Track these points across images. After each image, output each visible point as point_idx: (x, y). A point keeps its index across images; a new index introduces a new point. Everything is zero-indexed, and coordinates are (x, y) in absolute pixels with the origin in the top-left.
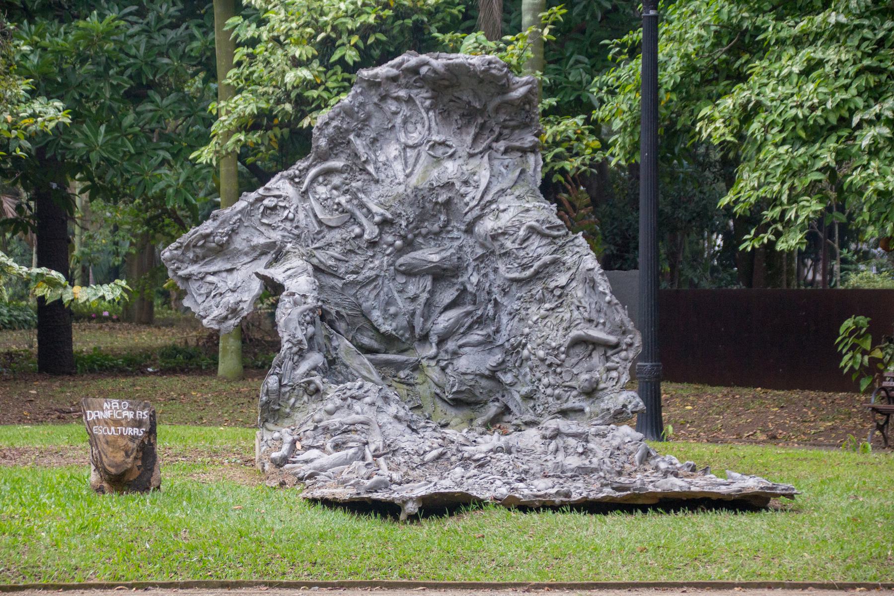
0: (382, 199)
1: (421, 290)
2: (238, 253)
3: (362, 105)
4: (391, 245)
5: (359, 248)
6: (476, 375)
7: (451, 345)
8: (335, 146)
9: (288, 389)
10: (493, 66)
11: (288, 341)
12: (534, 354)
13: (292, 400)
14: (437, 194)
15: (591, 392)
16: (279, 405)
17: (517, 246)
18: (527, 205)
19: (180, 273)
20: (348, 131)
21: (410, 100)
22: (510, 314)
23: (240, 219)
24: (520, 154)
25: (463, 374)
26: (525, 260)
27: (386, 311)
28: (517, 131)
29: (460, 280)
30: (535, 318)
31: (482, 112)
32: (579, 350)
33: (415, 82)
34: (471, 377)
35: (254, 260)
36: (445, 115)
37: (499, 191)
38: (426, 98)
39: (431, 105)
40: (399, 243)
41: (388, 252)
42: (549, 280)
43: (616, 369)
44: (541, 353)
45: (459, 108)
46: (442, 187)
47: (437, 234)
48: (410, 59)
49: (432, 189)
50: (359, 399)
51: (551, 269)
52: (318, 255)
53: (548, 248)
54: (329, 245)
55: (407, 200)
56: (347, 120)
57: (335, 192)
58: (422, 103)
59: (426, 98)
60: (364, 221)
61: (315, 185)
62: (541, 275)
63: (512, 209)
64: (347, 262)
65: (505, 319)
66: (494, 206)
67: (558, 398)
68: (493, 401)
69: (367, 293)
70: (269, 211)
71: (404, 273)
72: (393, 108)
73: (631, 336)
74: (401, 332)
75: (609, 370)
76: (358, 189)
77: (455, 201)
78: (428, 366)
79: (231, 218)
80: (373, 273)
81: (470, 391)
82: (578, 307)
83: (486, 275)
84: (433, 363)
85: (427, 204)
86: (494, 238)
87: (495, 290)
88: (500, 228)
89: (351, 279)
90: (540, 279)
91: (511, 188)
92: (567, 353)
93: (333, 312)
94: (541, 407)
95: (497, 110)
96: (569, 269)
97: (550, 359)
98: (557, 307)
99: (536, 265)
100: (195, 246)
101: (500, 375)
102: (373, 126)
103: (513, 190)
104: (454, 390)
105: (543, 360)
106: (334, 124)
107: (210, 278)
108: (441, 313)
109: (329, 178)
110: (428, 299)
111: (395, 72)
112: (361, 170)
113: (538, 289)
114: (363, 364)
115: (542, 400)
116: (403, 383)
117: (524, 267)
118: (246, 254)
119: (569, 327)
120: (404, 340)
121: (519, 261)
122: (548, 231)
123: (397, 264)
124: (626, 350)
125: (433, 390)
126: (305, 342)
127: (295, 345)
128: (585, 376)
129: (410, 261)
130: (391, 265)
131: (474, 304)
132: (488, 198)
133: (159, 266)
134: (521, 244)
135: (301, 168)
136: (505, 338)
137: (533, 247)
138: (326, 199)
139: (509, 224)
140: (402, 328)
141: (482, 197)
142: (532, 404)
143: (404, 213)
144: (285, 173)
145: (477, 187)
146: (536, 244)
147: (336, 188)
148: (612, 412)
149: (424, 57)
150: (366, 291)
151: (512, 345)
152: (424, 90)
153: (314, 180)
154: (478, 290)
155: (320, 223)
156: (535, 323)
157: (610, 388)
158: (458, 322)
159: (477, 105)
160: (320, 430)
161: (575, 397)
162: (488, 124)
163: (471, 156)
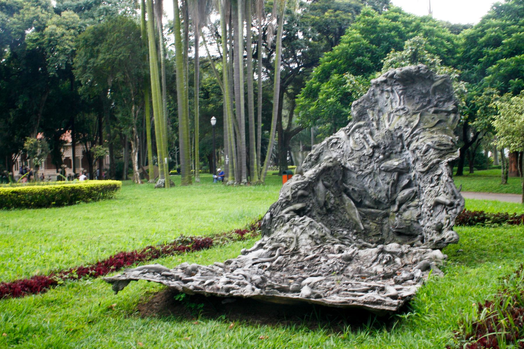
4: (378, 157)
6: (412, 221)
7: (404, 206)
20: (367, 108)
21: (392, 91)
23: (323, 148)
28: (446, 103)
34: (409, 222)
38: (400, 90)
58: (398, 93)
59: (400, 90)
66: (417, 137)
74: (383, 199)
90: (432, 171)
106: (362, 104)
108: (401, 191)
111: (384, 79)
114: (355, 213)
116: (376, 223)
132: (415, 132)
140: (384, 197)
144: (344, 128)
148: (435, 241)
150: (366, 179)
152: (399, 86)
153: (354, 131)
155: (352, 150)
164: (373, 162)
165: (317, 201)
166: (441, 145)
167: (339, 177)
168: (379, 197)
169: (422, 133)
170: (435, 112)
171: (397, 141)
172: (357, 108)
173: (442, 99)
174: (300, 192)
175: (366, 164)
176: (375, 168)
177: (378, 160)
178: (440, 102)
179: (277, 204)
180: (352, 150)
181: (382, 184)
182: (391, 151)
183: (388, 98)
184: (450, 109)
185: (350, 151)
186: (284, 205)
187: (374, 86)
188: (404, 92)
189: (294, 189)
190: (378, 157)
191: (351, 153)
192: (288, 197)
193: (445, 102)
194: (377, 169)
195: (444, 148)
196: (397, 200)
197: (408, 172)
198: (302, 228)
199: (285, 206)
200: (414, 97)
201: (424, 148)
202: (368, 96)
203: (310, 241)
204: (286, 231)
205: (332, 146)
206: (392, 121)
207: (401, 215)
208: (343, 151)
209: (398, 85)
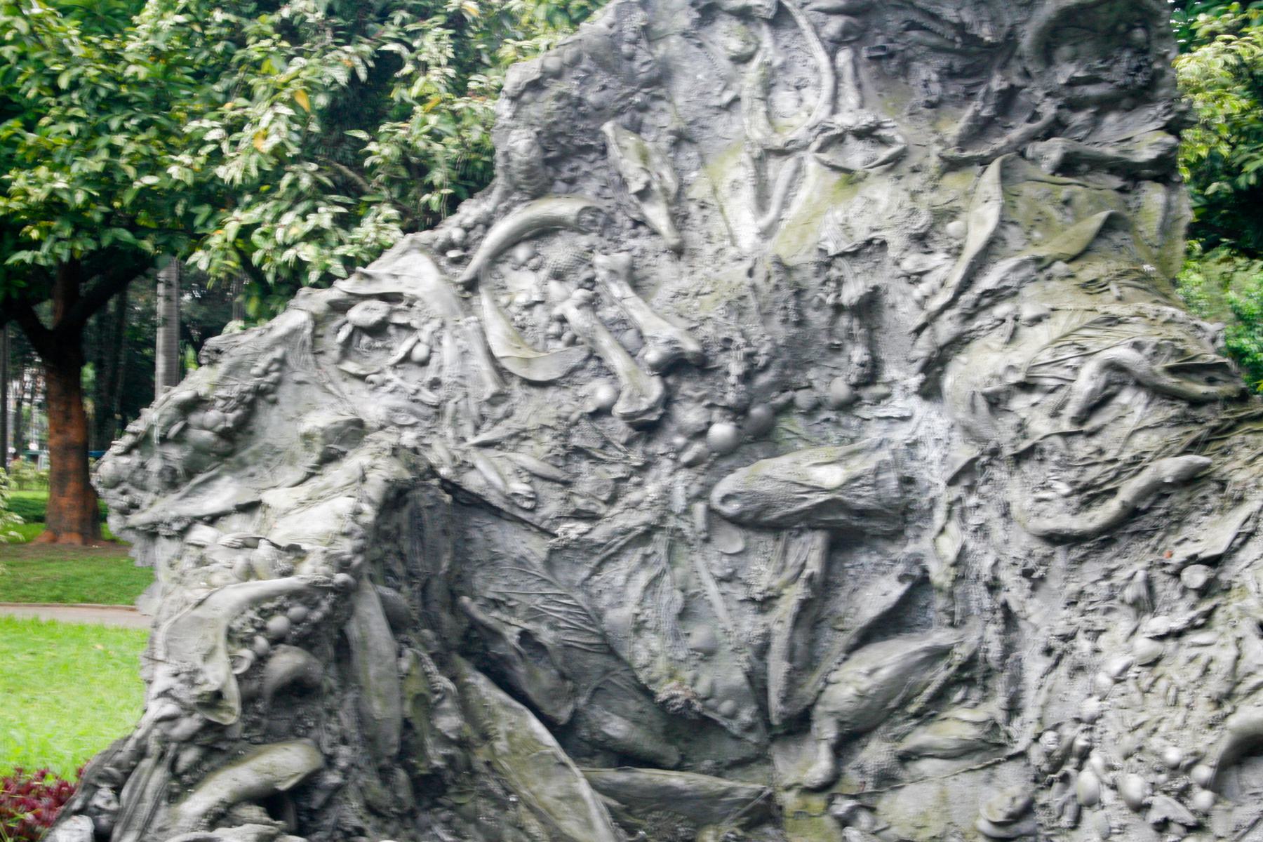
0: (682, 302)
2: (275, 456)
4: (701, 434)
5: (606, 444)
7: (875, 753)
8: (565, 156)
11: (165, 694)
14: (840, 282)
18: (1116, 310)
20: (601, 112)
23: (282, 362)
24: (1117, 182)
28: (1111, 118)
29: (911, 548)
30: (1116, 665)
31: (1006, 47)
39: (845, 32)
40: (722, 430)
41: (686, 457)
42: (1172, 539)
44: (1135, 785)
45: (936, 49)
46: (854, 255)
47: (847, 406)
49: (826, 263)
51: (1178, 500)
53: (1174, 434)
54: (520, 436)
56: (601, 78)
58: (816, 29)
60: (617, 360)
61: (505, 268)
62: (1144, 523)
65: (1034, 666)
66: (1002, 310)
69: (620, 579)
70: (366, 339)
71: (737, 521)
72: (735, 45)
74: (727, 706)
77: (889, 299)
83: (982, 531)
84: (817, 802)
85: (811, 314)
88: (1011, 368)
89: (573, 535)
90: (1140, 534)
92: (1216, 785)
96: (1240, 500)
97: (1164, 807)
98: (1193, 627)
99: (1129, 489)
102: (680, 101)
103: (1073, 267)
105: (1140, 808)
106: (569, 85)
108: (851, 650)
114: (575, 798)
117: (1090, 495)
119: (1229, 696)
120: (735, 728)
121: (1072, 475)
127: (189, 711)
130: (698, 497)
132: (988, 281)
135: (469, 221)
136: (1031, 730)
140: (731, 693)
141: (967, 283)
143: (739, 340)
145: (956, 253)
147: (558, 276)
150: (616, 573)
151: (1049, 754)
153: (500, 255)
154: (958, 579)
155: (502, 374)
159: (986, 33)
162: (1022, 98)
164: (666, 464)
165: (362, 719)
166: (1187, 369)
167: (436, 556)
168: (702, 688)
169: (1029, 290)
170: (1068, 166)
171: (831, 332)
172: (533, 111)
173: (1092, 91)
174: (286, 662)
175: (618, 471)
176: (679, 503)
177: (698, 447)
178: (1074, 105)
179: (141, 753)
180: (502, 374)
181: (719, 606)
182: (781, 400)
183: (742, 59)
184: (1145, 154)
185: (491, 388)
186: (189, 756)
189: (248, 642)
190: (701, 434)
191: (497, 399)
193: (1105, 105)
194: (687, 511)
196: (819, 708)
197: (895, 536)
199: (195, 766)
200: (905, 68)
201: (1086, 382)
202: (613, 41)
206: (785, 204)
207: (872, 810)
208: (435, 384)
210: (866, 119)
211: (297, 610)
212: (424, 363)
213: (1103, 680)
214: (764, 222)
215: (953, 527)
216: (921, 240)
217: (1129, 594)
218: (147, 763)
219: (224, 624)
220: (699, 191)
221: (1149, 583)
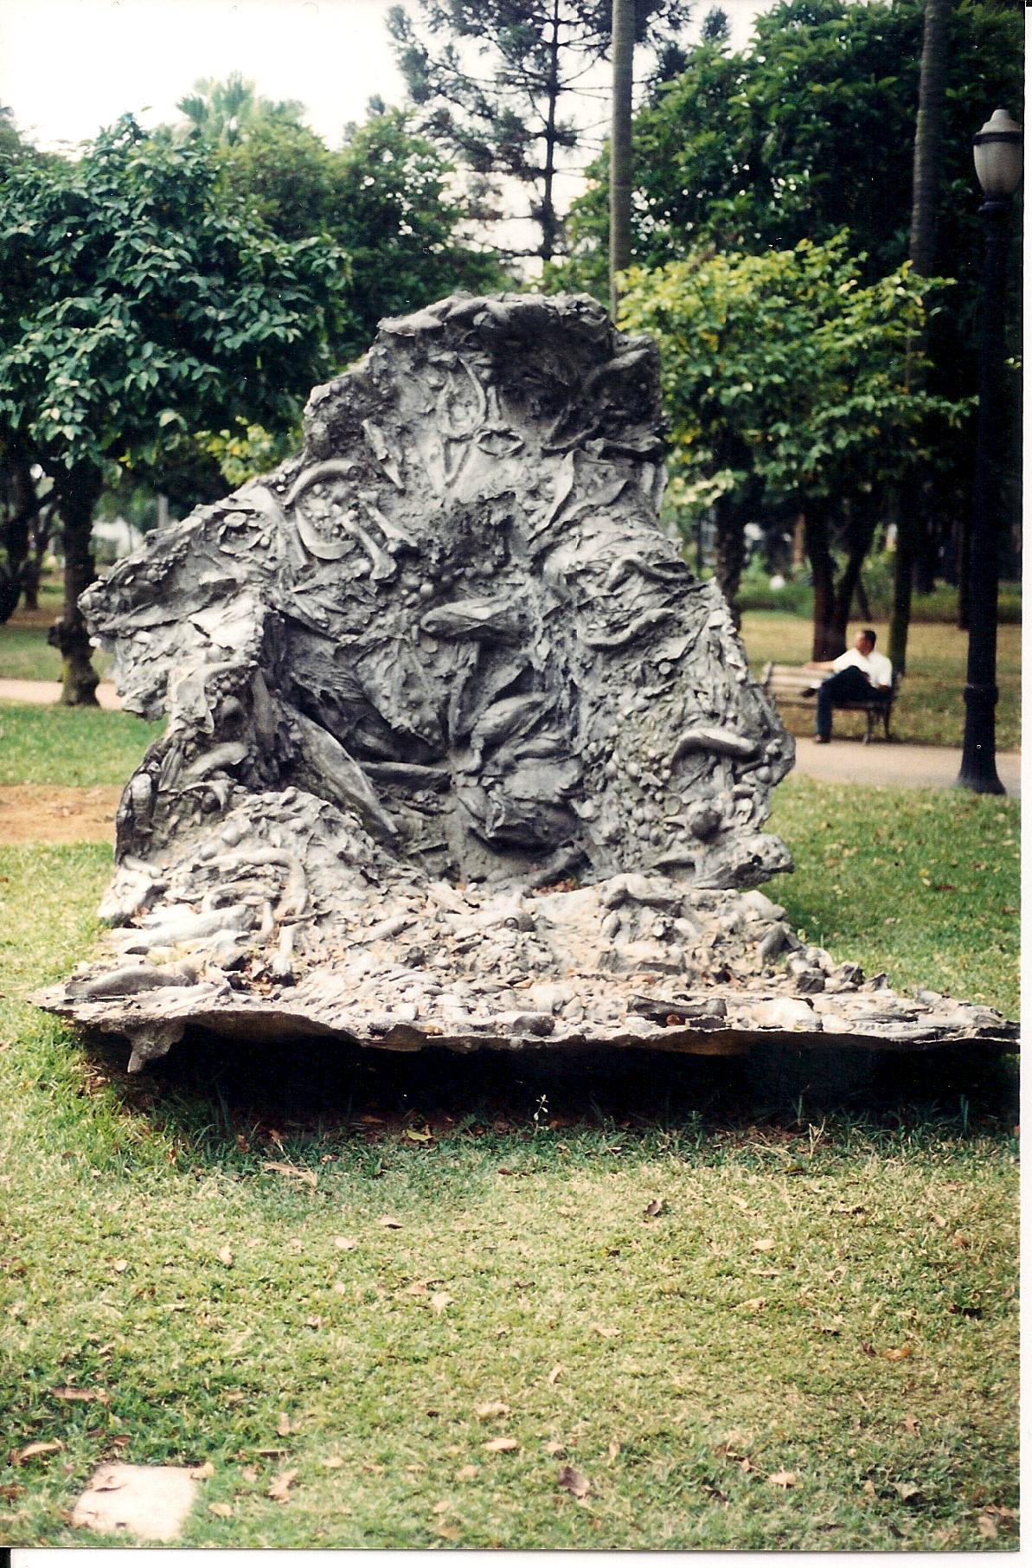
1: (460, 663)
3: (386, 373)
4: (415, 589)
5: (366, 593)
6: (539, 802)
7: (503, 754)
9: (170, 798)
10: (584, 309)
12: (624, 769)
13: (174, 819)
14: (490, 512)
15: (710, 832)
16: (151, 826)
17: (605, 593)
18: (630, 533)
19: (103, 627)
20: (361, 415)
21: (457, 369)
22: (592, 704)
23: (188, 544)
24: (630, 462)
25: (521, 800)
26: (617, 616)
27: (404, 695)
29: (524, 651)
32: (694, 766)
33: (468, 340)
34: (530, 805)
35: (204, 607)
36: (514, 396)
37: (584, 508)
40: (427, 588)
41: (408, 602)
42: (654, 650)
43: (749, 796)
44: (633, 768)
48: (459, 301)
49: (483, 503)
50: (282, 821)
52: (299, 603)
54: (320, 588)
55: (444, 522)
57: (336, 507)
58: (477, 375)
59: (484, 366)
60: (373, 549)
61: (309, 497)
62: (643, 641)
63: (603, 536)
64: (345, 614)
65: (585, 711)
66: (574, 531)
67: (657, 841)
68: (565, 846)
71: (434, 636)
72: (433, 381)
73: (777, 741)
74: (427, 731)
75: (738, 797)
76: (369, 503)
78: (465, 786)
79: (174, 541)
80: (382, 634)
81: (527, 827)
82: (696, 692)
83: (561, 643)
84: (473, 781)
85: (474, 529)
86: (571, 579)
87: (574, 666)
90: (642, 647)
91: (608, 505)
93: (316, 692)
94: (631, 858)
95: (596, 390)
96: (687, 632)
97: (649, 778)
99: (635, 624)
100: (122, 585)
101: (574, 804)
104: (499, 823)
105: (636, 779)
106: (345, 400)
107: (143, 636)
108: (491, 703)
109: (329, 488)
110: (468, 679)
111: (435, 322)
112: (379, 476)
113: (636, 665)
114: (352, 775)
115: (633, 845)
117: (615, 627)
118: (195, 598)
119: (680, 725)
121: (607, 617)
122: (657, 571)
123: (423, 622)
124: (769, 764)
125: (467, 824)
126: (210, 721)
127: (192, 726)
128: (698, 807)
129: (445, 617)
131: (544, 690)
132: (567, 516)
133: (1009, 908)
134: (613, 588)
137: (631, 596)
138: (323, 518)
139: (594, 558)
140: (431, 724)
141: (556, 517)
142: (619, 852)
144: (264, 478)
146: (636, 591)
147: (338, 502)
149: (480, 300)
150: (372, 661)
152: (481, 354)
153: (307, 489)
154: (548, 667)
155: (309, 555)
156: (628, 718)
157: (738, 828)
158: (517, 717)
160: (204, 873)
161: (682, 842)
162: (582, 416)
163: (547, 454)
169: (587, 521)
173: (618, 413)
182: (457, 572)
185: (304, 562)
186: (191, 747)
187: (390, 343)
188: (498, 378)
192: (201, 721)
195: (677, 576)
196: (474, 733)
198: (303, 831)
199: (193, 752)
203: (345, 873)
204: (233, 844)
205: (224, 539)
206: (460, 469)
208: (273, 559)
209: (479, 349)
210: (503, 426)
211: (234, 679)
212: (266, 548)
213: (620, 717)
214: (449, 478)
215: (545, 641)
216: (534, 493)
217: (634, 676)
218: (172, 751)
219: (202, 684)
220: (413, 459)
221: (643, 671)
